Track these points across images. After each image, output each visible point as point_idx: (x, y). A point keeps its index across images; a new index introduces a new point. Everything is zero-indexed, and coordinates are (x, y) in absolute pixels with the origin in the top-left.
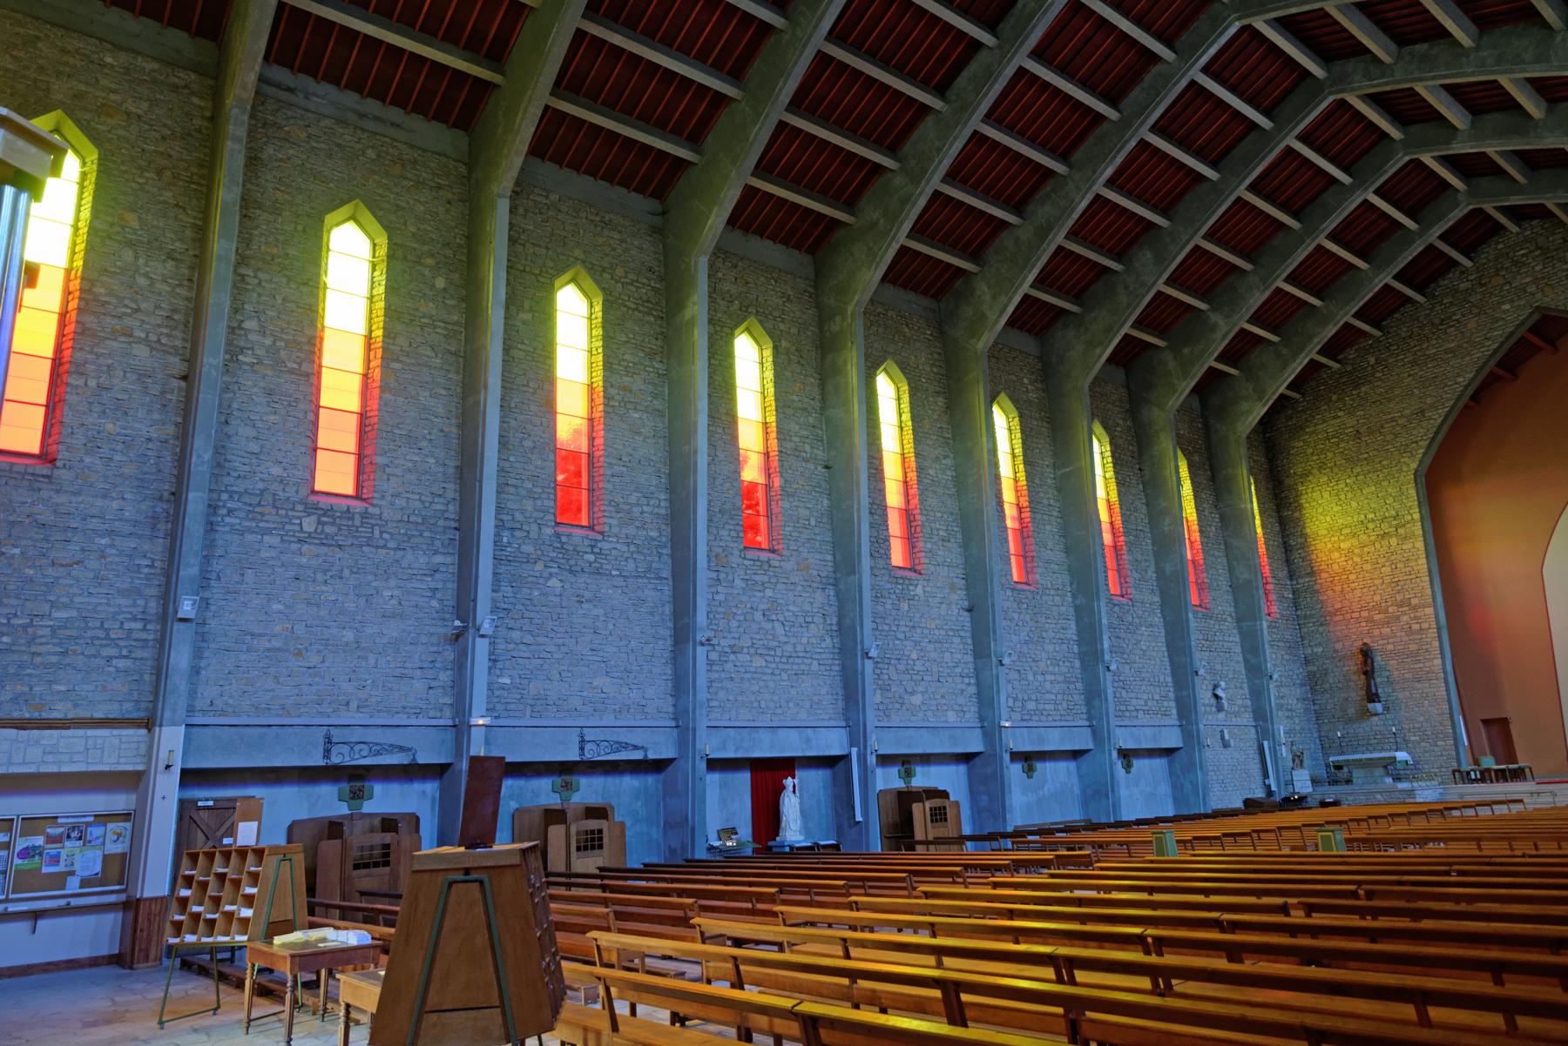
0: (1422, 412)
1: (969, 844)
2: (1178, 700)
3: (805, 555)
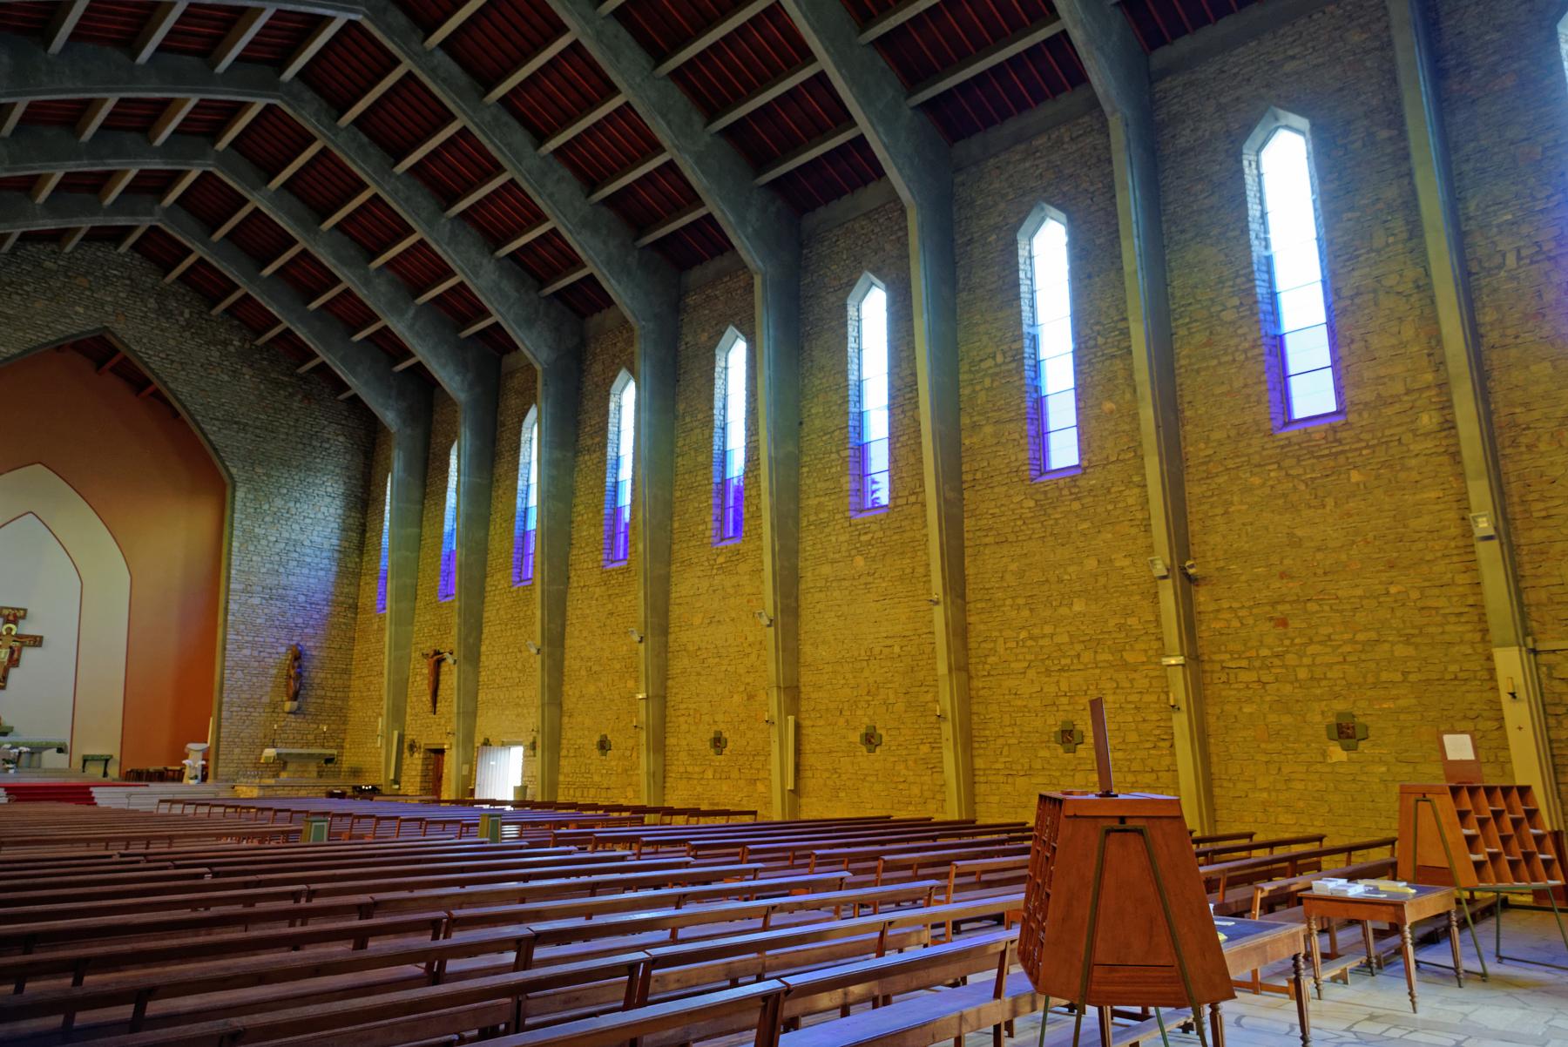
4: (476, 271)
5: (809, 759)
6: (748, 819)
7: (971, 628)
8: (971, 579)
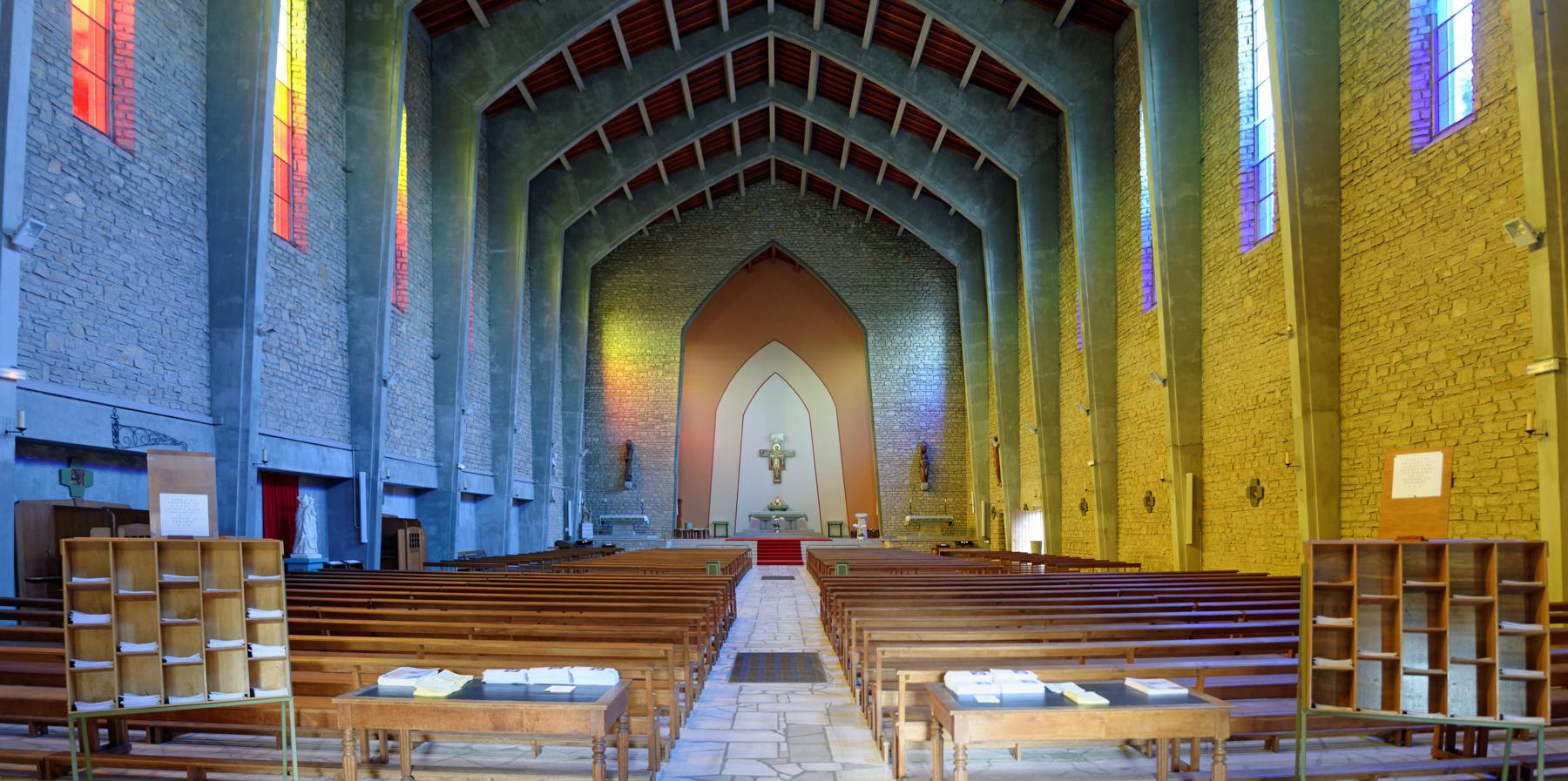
0: (695, 287)
2: (535, 464)
3: (324, 261)
4: (953, 111)
5: (1210, 516)
6: (1136, 570)
7: (1344, 359)
8: (1346, 300)
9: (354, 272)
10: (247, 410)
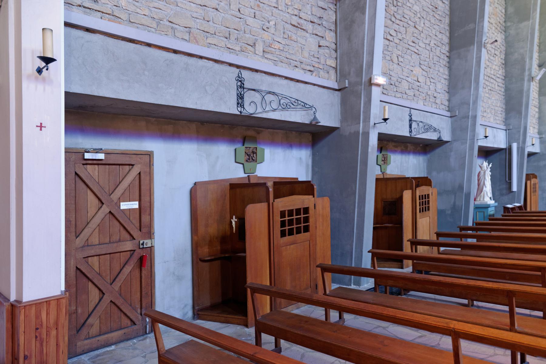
1: (75, 308)
9: (511, 10)
10: (475, 102)
